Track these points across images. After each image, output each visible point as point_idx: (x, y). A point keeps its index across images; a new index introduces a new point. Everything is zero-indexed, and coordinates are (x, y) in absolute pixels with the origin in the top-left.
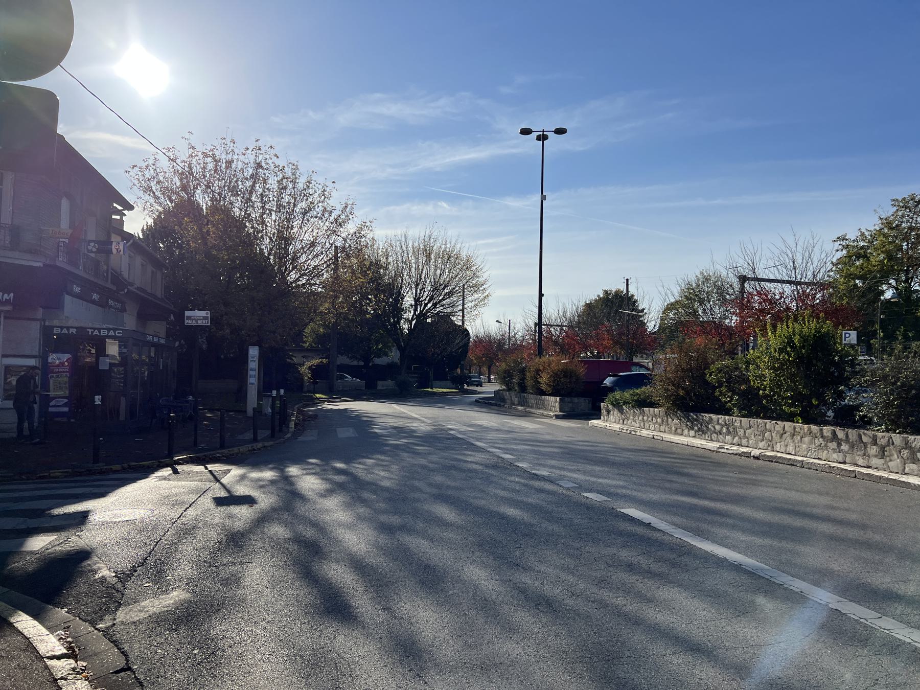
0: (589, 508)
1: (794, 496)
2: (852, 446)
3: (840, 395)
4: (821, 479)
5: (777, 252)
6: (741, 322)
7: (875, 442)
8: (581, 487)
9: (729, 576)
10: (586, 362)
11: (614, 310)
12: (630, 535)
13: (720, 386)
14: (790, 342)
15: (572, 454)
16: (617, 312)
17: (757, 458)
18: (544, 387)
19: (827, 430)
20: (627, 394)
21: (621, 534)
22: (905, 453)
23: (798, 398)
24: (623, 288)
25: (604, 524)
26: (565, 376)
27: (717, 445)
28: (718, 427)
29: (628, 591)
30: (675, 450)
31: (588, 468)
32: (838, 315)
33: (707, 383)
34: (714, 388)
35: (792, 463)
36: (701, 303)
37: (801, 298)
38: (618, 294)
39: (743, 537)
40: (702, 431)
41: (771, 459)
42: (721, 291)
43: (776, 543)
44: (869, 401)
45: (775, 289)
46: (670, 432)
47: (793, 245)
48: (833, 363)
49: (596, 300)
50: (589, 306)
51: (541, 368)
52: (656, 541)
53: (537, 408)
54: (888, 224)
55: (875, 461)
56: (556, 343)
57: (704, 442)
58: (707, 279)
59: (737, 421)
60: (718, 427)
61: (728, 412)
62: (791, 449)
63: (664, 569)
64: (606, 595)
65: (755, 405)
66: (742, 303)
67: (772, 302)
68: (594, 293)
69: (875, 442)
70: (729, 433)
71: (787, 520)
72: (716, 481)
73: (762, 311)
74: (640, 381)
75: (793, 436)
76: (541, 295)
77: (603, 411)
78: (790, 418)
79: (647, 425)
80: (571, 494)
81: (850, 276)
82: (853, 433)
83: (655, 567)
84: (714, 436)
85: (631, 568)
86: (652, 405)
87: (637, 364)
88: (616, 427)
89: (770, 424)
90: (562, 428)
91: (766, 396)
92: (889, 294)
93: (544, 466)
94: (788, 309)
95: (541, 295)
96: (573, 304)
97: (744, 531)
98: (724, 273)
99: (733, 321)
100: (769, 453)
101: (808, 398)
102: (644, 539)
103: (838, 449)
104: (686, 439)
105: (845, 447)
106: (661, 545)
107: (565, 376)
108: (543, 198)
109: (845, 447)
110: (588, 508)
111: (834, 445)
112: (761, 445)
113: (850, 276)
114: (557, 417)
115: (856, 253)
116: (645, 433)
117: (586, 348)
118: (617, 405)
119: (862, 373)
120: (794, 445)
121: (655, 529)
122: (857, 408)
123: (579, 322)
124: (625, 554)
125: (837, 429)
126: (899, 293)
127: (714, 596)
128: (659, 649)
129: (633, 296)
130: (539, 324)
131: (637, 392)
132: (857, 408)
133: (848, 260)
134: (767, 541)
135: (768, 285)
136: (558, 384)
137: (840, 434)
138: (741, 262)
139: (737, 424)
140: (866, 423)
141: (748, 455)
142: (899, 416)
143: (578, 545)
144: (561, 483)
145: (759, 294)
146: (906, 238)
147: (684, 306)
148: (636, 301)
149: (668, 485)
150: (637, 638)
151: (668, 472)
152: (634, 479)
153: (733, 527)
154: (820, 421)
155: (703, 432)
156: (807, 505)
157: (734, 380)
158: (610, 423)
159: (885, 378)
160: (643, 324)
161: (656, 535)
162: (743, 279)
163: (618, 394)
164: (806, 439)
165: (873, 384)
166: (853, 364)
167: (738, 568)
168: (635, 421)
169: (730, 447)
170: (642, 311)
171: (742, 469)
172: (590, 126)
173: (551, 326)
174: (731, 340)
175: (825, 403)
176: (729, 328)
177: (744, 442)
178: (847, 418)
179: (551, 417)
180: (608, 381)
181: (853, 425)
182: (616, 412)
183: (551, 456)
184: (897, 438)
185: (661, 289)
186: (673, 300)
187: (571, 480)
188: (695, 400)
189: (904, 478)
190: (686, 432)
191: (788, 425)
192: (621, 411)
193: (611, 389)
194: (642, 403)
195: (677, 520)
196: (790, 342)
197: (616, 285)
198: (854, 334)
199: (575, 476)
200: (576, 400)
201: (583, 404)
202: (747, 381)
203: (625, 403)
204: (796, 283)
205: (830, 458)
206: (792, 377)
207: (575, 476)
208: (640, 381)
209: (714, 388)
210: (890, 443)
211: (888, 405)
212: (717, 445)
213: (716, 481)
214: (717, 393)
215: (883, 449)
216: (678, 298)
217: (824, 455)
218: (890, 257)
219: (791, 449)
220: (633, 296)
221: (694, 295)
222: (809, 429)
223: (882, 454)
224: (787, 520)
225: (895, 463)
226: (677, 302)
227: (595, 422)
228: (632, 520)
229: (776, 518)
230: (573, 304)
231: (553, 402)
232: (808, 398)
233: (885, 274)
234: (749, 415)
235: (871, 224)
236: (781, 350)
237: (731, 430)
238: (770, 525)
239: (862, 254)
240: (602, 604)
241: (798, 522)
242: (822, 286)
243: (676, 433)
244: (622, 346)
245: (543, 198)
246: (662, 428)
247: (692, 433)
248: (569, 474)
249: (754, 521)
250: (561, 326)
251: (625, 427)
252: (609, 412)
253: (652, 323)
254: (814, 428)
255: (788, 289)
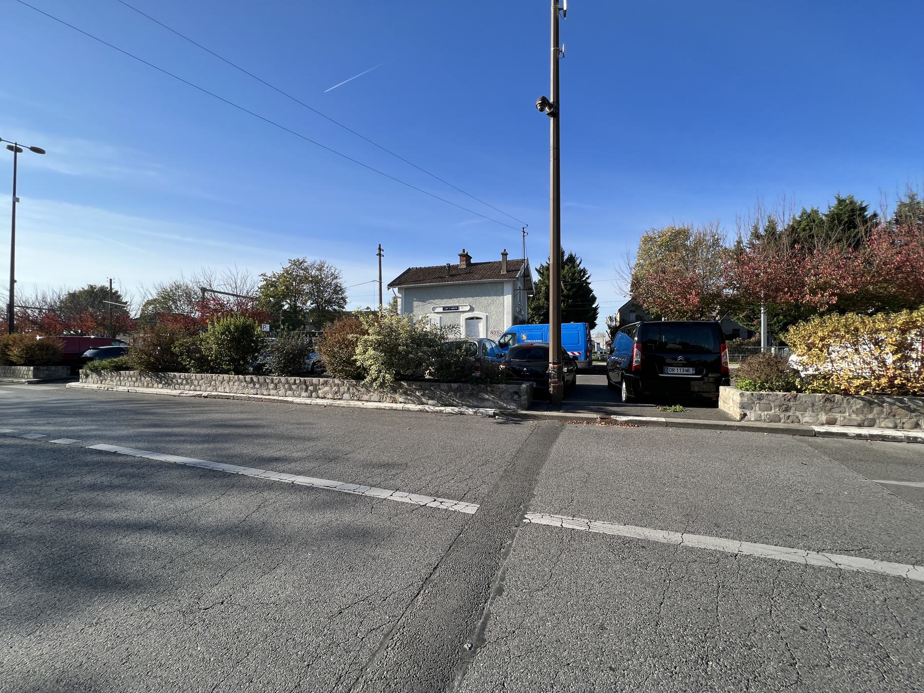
0: (58, 451)
1: (228, 416)
2: (261, 385)
3: (256, 359)
4: (242, 405)
5: (225, 276)
6: (202, 316)
7: (272, 382)
8: (49, 436)
9: (175, 473)
10: (64, 339)
11: (101, 301)
12: (98, 464)
13: (182, 354)
14: (228, 329)
15: (40, 411)
16: (101, 302)
17: (206, 397)
18: (14, 359)
19: (248, 378)
20: (105, 362)
21: (87, 465)
22: (286, 386)
23: (232, 360)
24: (107, 285)
25: (75, 460)
26: (39, 349)
27: (179, 391)
28: (179, 381)
29: (87, 505)
30: (147, 398)
31: (60, 420)
32: (258, 316)
33: (173, 354)
34: (178, 356)
35: (228, 398)
36: (174, 303)
37: (239, 304)
38: (102, 289)
39: (189, 446)
40: (168, 384)
41: (215, 397)
42: (188, 295)
43: (211, 446)
44: (271, 361)
45: (225, 298)
46: (143, 386)
47: (235, 274)
48: (253, 341)
49: (80, 292)
50: (73, 296)
51: (11, 343)
52: (120, 463)
53: (6, 377)
54: (287, 272)
55: (272, 392)
56: (34, 322)
57: (169, 391)
58: (178, 287)
59: (193, 376)
60: (179, 381)
61: (187, 371)
62: (227, 390)
63: (125, 481)
64: (64, 515)
65: (206, 366)
66: (203, 304)
67: (222, 305)
68: (78, 283)
69: (272, 382)
70: (187, 383)
71: (221, 431)
72: (175, 415)
73: (216, 310)
74: (118, 352)
75: (228, 382)
76: (13, 281)
77: (82, 376)
78: (227, 372)
79: (123, 383)
80: (37, 443)
81: (267, 296)
82: (261, 378)
83: (116, 482)
84: (177, 386)
85: (92, 487)
86: (127, 369)
87: (120, 342)
88: (95, 386)
89: (214, 376)
90: (36, 391)
91: (212, 360)
92: (286, 307)
93: (7, 425)
94: (232, 310)
95: (13, 281)
96: (54, 292)
97: (191, 442)
98: (190, 286)
99: (197, 315)
100: (213, 393)
101: (238, 360)
102: (108, 462)
103: (254, 388)
104: (158, 390)
105: (257, 386)
106: (124, 465)
107: (39, 349)
108: (15, 200)
109: (257, 386)
110: (54, 452)
111: (252, 385)
112: (209, 389)
113: (267, 296)
114: (30, 383)
115: (270, 284)
116: (121, 388)
117: (68, 328)
118: (96, 370)
119: (267, 346)
120: (229, 387)
121: (120, 455)
122: (264, 365)
123: (60, 308)
124: (89, 479)
125: (254, 377)
126: (291, 308)
127: (163, 489)
128: (128, 541)
129: (117, 292)
130: (11, 306)
131: (113, 359)
132: (264, 365)
133: (266, 287)
134: (206, 446)
135: (220, 295)
136: (32, 356)
137: (255, 379)
138: (202, 279)
139: (193, 378)
140: (268, 373)
141: (200, 396)
142: (284, 368)
143: (39, 483)
144: (25, 436)
145: (214, 300)
146: (295, 280)
147: (160, 303)
148: (119, 296)
149: (136, 423)
150: (90, 537)
151: (138, 414)
152: (106, 423)
153: (184, 441)
154: (244, 373)
155: (169, 385)
156: (234, 420)
157: (191, 352)
158: (89, 384)
159: (278, 349)
160: (126, 314)
161: (120, 459)
162: (204, 290)
163: (96, 363)
164: (236, 384)
165: (272, 352)
166: (262, 341)
167: (183, 466)
168: (112, 381)
169: (220, 392)
170: (126, 303)
171: (192, 405)
172: (62, 157)
173: (28, 308)
174: (193, 327)
175: (248, 363)
176: (193, 319)
177: (198, 388)
178: (259, 370)
179: (23, 383)
180: (88, 353)
181: (264, 374)
182: (94, 375)
183: (16, 416)
184: (283, 379)
185: (141, 290)
186: (150, 298)
187: (37, 432)
188: (162, 364)
189: (285, 399)
190: (156, 385)
191: (226, 376)
192: (99, 374)
193: (91, 359)
194: (118, 368)
195: (140, 445)
196: (228, 329)
197: (100, 282)
198: (268, 326)
199: (44, 428)
200: (53, 368)
201: (62, 371)
202: (200, 351)
203: (103, 369)
204: (237, 296)
205: (250, 392)
206: (229, 349)
207: (44, 428)
208: (118, 352)
209: (178, 356)
210: (280, 382)
211: (279, 362)
212: (179, 391)
213: (175, 415)
214: (179, 359)
215: (276, 385)
216: (155, 297)
217: (246, 391)
218: (287, 288)
219: (227, 390)
220: (117, 292)
221: (168, 297)
222: (252, 379)
223: (276, 388)
224: (221, 431)
225: (282, 392)
226: (155, 300)
227: (73, 384)
228: (100, 452)
229: (214, 431)
230: (54, 292)
231: (27, 371)
232: (238, 360)
233: (285, 297)
234: (202, 372)
235: (279, 270)
236: (222, 334)
237: (189, 382)
238: (208, 435)
239: (273, 284)
240: (60, 522)
241: (226, 431)
242: (252, 299)
243: (148, 386)
244: (105, 327)
245: (15, 200)
246: (136, 384)
247: (160, 386)
248: (37, 428)
249: (199, 435)
250: (40, 309)
251: (103, 386)
252: (87, 376)
253: (134, 312)
254: (241, 377)
255: (232, 298)
